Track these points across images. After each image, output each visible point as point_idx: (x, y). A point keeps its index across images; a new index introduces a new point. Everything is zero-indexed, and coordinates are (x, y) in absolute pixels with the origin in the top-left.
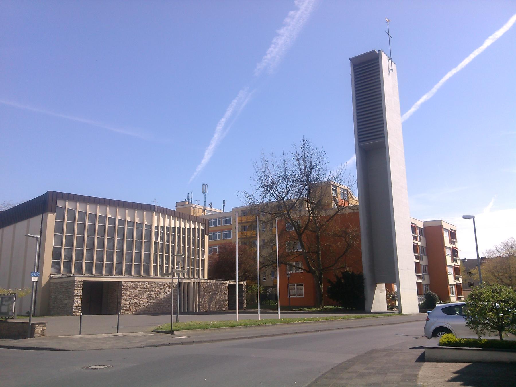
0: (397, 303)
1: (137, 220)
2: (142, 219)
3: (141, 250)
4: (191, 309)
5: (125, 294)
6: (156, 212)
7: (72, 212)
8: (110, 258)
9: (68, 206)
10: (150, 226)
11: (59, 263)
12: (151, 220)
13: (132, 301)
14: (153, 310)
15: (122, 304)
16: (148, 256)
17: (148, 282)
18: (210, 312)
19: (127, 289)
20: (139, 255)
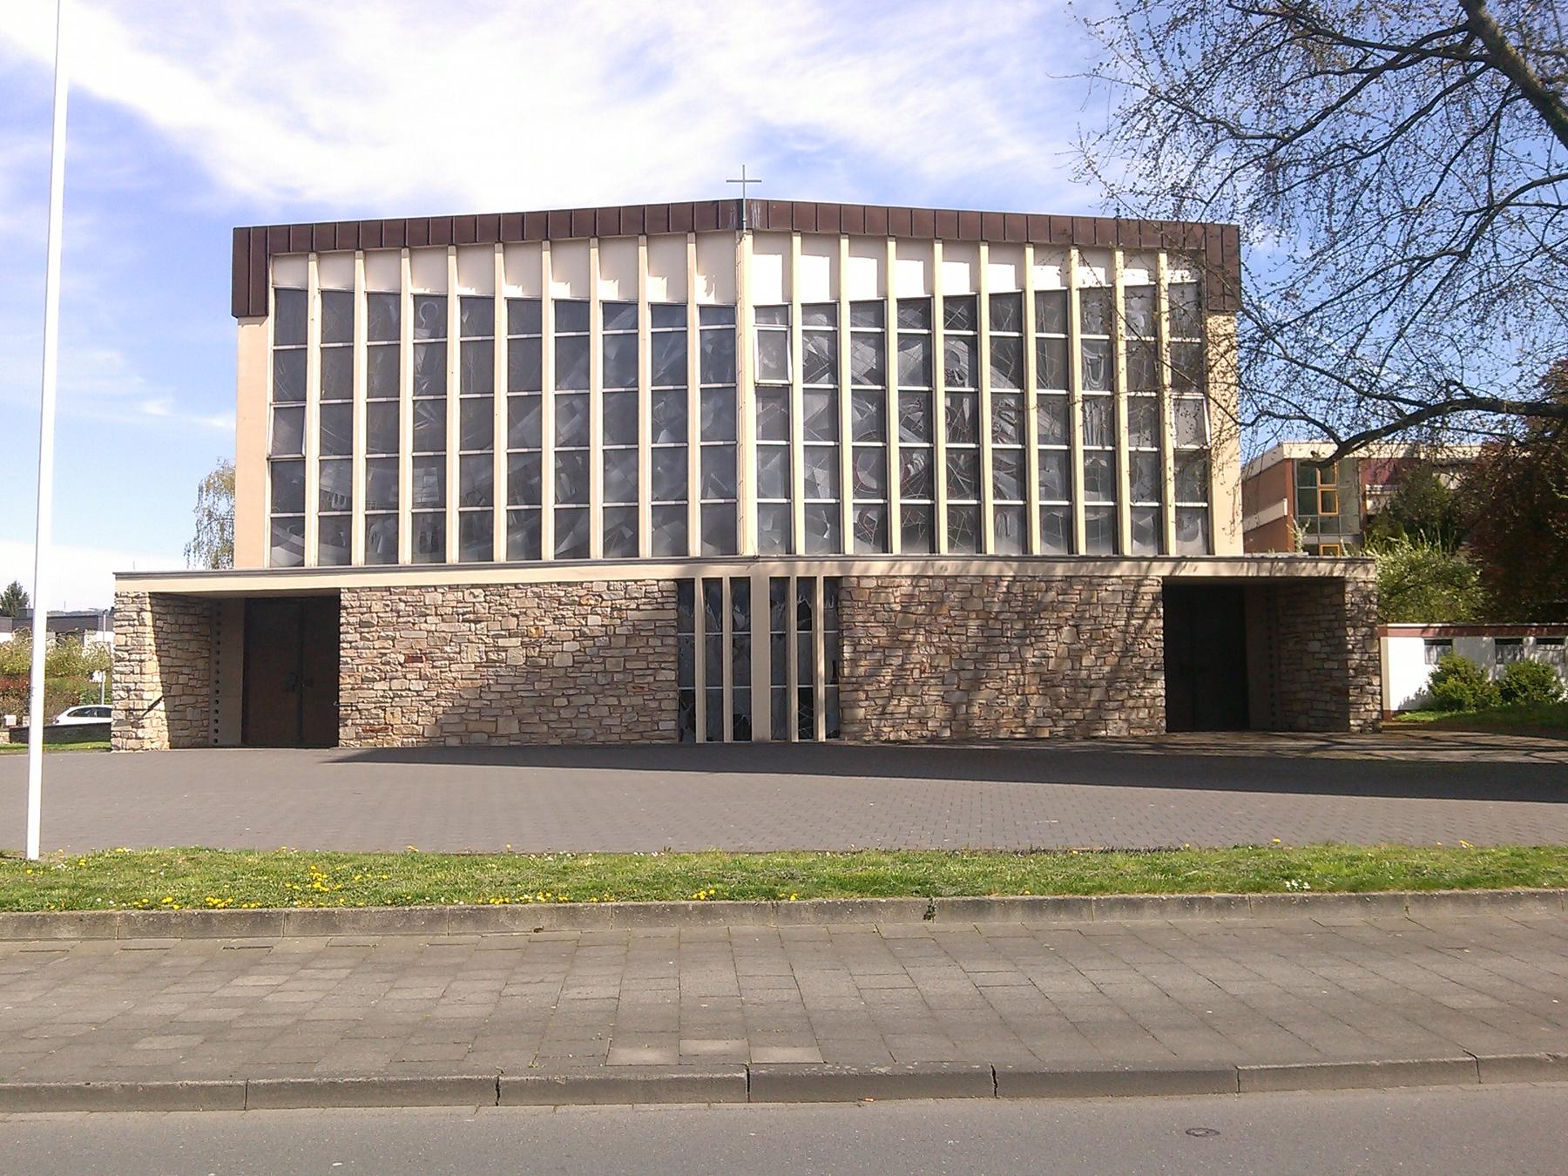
0: (1376, 681)
1: (701, 293)
2: (680, 281)
3: (679, 430)
4: (761, 727)
5: (356, 652)
6: (755, 233)
7: (338, 303)
8: (525, 484)
9: (317, 277)
10: (722, 315)
11: (298, 527)
12: (728, 277)
13: (396, 684)
14: (514, 728)
15: (344, 697)
16: (723, 463)
17: (484, 587)
18: (959, 756)
19: (362, 624)
20: (671, 464)
